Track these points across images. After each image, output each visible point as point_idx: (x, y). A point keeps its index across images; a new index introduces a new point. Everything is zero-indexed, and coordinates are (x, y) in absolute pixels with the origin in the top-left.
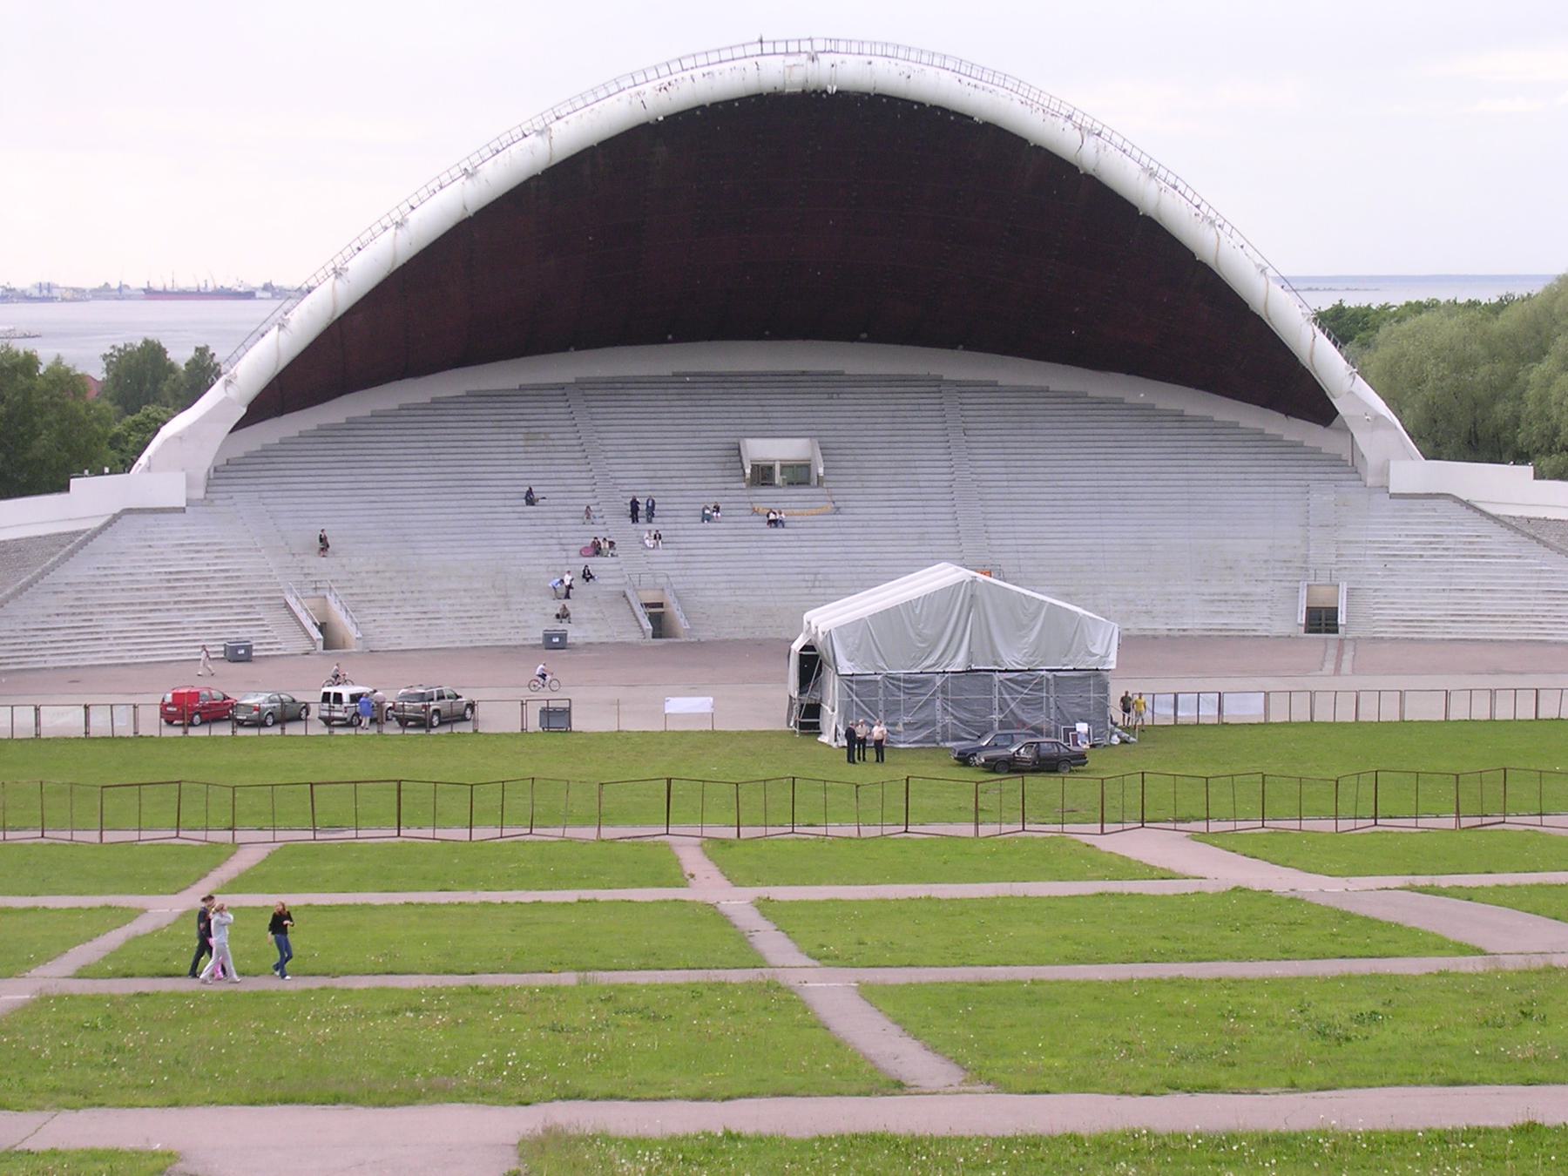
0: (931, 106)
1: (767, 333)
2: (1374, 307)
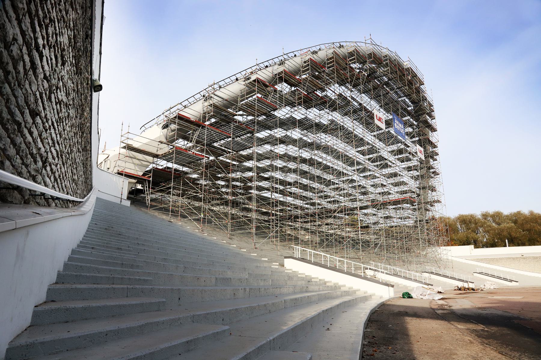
2: (473, 246)
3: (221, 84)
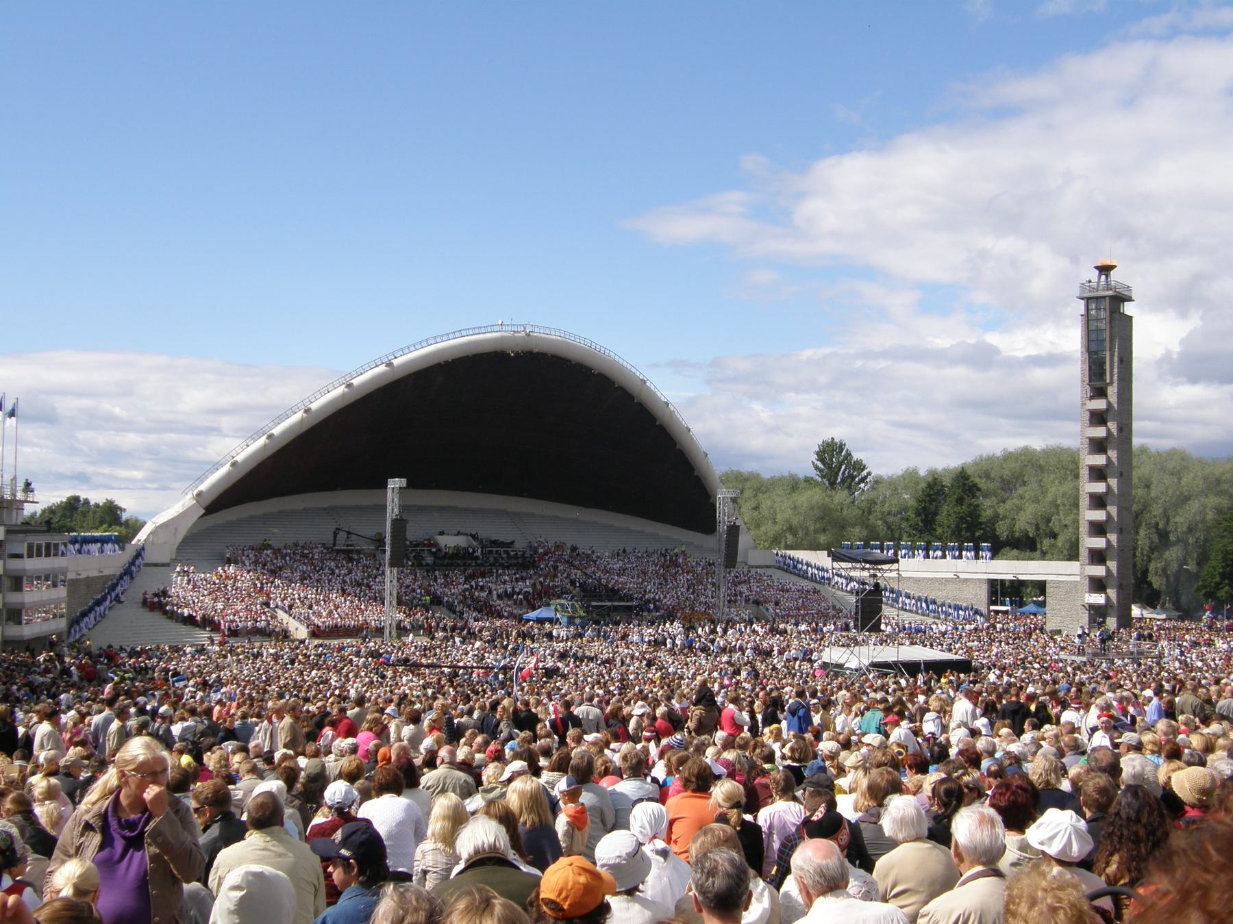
0: (517, 354)
1: (481, 487)
3: (231, 454)
